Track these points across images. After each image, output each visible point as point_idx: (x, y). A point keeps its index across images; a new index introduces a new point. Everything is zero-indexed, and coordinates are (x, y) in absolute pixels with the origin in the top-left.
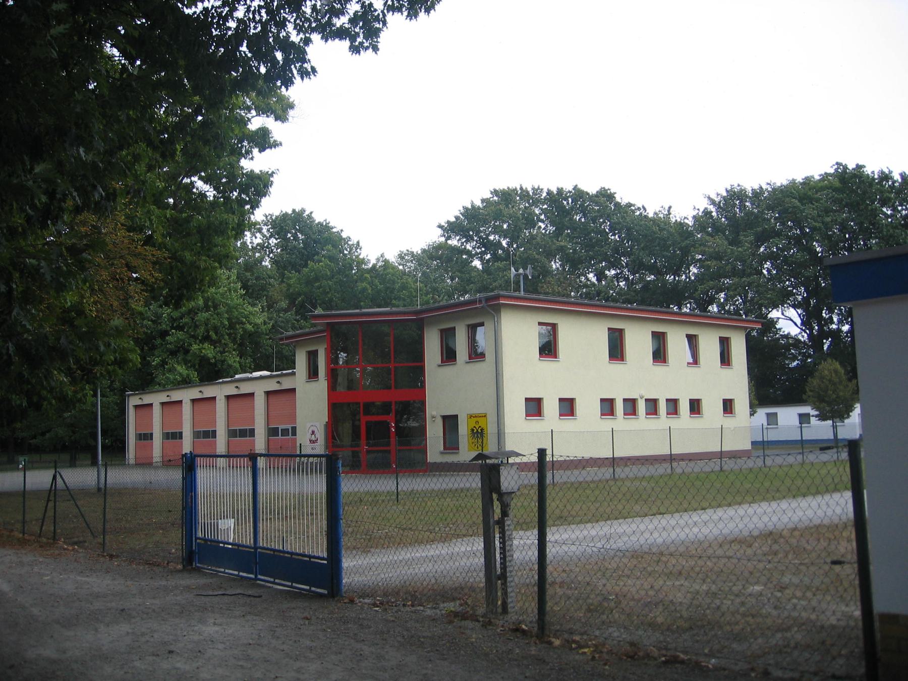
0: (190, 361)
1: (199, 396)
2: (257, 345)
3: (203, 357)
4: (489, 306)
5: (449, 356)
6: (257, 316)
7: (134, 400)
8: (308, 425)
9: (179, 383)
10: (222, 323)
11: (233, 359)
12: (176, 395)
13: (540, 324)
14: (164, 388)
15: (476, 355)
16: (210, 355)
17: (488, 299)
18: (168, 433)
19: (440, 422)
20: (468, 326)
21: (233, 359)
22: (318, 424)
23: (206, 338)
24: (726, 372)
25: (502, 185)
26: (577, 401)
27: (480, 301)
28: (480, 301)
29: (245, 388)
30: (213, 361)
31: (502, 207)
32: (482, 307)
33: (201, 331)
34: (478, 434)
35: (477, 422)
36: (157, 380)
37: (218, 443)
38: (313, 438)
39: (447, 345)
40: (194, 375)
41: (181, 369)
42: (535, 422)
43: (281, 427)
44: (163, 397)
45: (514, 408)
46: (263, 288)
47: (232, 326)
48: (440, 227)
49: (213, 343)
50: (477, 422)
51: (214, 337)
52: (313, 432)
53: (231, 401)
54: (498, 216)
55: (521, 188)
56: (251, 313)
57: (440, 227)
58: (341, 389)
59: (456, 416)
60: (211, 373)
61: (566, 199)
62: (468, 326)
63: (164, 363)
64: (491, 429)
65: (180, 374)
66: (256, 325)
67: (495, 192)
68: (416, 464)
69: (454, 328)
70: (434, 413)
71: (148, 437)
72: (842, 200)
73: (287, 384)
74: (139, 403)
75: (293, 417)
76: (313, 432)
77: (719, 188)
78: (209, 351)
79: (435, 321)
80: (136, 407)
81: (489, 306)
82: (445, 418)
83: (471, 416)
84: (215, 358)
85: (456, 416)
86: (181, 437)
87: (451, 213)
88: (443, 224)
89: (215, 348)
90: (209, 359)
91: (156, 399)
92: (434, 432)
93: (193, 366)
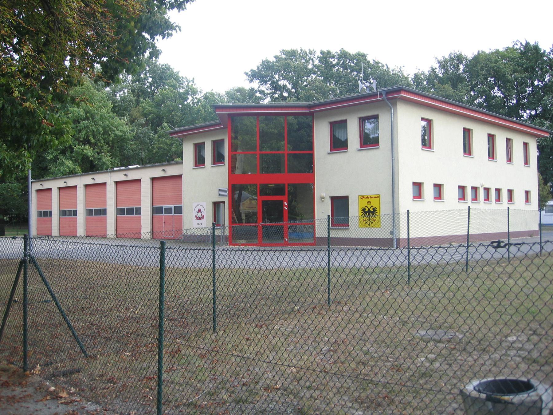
0: (74, 157)
1: (92, 182)
2: (121, 148)
3: (84, 155)
4: (388, 99)
5: (339, 144)
6: (122, 126)
7: (34, 186)
8: (195, 204)
9: (69, 173)
10: (98, 130)
11: (106, 159)
12: (71, 182)
13: (423, 119)
14: (55, 177)
15: (369, 142)
16: (90, 154)
17: (388, 93)
18: (41, 212)
19: (328, 202)
20: (360, 118)
21: (106, 159)
22: (204, 204)
23: (86, 141)
24: (526, 169)
25: (288, 48)
26: (445, 186)
27: (381, 95)
28: (381, 95)
29: (133, 175)
30: (92, 159)
31: (288, 61)
32: (382, 100)
33: (83, 134)
34: (369, 213)
35: (369, 202)
36: (51, 171)
37: (142, 218)
38: (199, 215)
39: (335, 136)
40: (79, 169)
41: (69, 163)
42: (419, 202)
43: (164, 206)
44: (60, 183)
45: (405, 191)
46: (126, 109)
47: (105, 133)
48: (246, 74)
49: (93, 146)
50: (369, 202)
51: (93, 140)
52: (199, 211)
53: (120, 186)
54: (287, 67)
55: (301, 50)
56: (120, 124)
57: (246, 74)
58: (238, 172)
59: (346, 198)
60: (90, 167)
61: (333, 57)
62: (360, 118)
63: (55, 159)
64: (384, 210)
65: (69, 167)
66: (124, 132)
67: (284, 52)
68: (306, 239)
69: (345, 121)
70: (323, 194)
71: (48, 214)
72: (523, 64)
73: (172, 171)
74: (40, 188)
75: (180, 198)
76: (199, 211)
77: (445, 52)
78: (89, 151)
79: (325, 114)
80: (38, 191)
81: (388, 99)
82: (333, 199)
83: (362, 197)
84: (93, 156)
85: (346, 198)
86: (50, 215)
87: (255, 65)
88: (247, 71)
89: (94, 149)
90: (88, 157)
91: (54, 185)
92: (322, 211)
93: (76, 161)
